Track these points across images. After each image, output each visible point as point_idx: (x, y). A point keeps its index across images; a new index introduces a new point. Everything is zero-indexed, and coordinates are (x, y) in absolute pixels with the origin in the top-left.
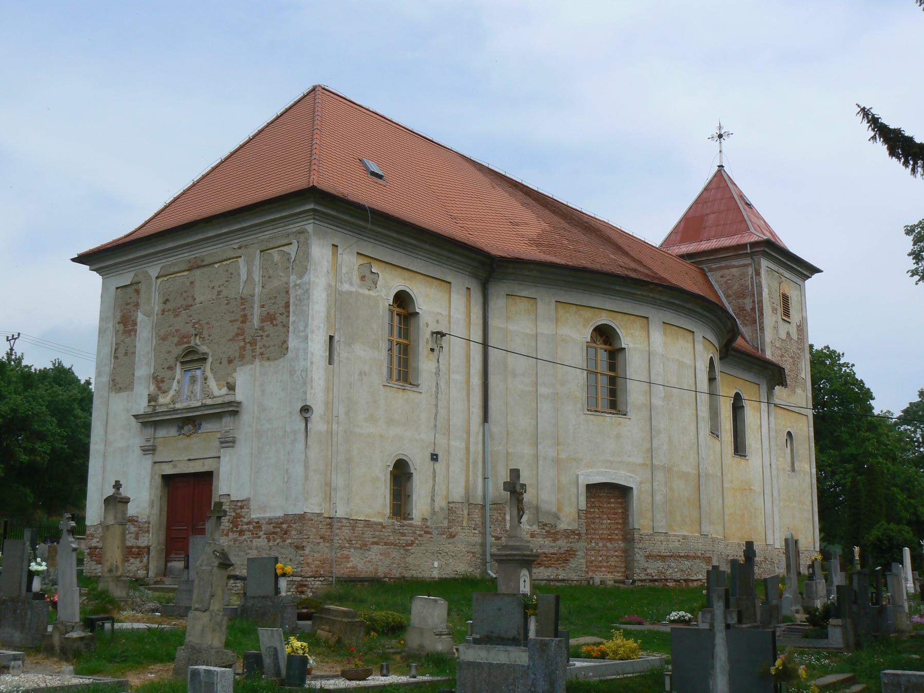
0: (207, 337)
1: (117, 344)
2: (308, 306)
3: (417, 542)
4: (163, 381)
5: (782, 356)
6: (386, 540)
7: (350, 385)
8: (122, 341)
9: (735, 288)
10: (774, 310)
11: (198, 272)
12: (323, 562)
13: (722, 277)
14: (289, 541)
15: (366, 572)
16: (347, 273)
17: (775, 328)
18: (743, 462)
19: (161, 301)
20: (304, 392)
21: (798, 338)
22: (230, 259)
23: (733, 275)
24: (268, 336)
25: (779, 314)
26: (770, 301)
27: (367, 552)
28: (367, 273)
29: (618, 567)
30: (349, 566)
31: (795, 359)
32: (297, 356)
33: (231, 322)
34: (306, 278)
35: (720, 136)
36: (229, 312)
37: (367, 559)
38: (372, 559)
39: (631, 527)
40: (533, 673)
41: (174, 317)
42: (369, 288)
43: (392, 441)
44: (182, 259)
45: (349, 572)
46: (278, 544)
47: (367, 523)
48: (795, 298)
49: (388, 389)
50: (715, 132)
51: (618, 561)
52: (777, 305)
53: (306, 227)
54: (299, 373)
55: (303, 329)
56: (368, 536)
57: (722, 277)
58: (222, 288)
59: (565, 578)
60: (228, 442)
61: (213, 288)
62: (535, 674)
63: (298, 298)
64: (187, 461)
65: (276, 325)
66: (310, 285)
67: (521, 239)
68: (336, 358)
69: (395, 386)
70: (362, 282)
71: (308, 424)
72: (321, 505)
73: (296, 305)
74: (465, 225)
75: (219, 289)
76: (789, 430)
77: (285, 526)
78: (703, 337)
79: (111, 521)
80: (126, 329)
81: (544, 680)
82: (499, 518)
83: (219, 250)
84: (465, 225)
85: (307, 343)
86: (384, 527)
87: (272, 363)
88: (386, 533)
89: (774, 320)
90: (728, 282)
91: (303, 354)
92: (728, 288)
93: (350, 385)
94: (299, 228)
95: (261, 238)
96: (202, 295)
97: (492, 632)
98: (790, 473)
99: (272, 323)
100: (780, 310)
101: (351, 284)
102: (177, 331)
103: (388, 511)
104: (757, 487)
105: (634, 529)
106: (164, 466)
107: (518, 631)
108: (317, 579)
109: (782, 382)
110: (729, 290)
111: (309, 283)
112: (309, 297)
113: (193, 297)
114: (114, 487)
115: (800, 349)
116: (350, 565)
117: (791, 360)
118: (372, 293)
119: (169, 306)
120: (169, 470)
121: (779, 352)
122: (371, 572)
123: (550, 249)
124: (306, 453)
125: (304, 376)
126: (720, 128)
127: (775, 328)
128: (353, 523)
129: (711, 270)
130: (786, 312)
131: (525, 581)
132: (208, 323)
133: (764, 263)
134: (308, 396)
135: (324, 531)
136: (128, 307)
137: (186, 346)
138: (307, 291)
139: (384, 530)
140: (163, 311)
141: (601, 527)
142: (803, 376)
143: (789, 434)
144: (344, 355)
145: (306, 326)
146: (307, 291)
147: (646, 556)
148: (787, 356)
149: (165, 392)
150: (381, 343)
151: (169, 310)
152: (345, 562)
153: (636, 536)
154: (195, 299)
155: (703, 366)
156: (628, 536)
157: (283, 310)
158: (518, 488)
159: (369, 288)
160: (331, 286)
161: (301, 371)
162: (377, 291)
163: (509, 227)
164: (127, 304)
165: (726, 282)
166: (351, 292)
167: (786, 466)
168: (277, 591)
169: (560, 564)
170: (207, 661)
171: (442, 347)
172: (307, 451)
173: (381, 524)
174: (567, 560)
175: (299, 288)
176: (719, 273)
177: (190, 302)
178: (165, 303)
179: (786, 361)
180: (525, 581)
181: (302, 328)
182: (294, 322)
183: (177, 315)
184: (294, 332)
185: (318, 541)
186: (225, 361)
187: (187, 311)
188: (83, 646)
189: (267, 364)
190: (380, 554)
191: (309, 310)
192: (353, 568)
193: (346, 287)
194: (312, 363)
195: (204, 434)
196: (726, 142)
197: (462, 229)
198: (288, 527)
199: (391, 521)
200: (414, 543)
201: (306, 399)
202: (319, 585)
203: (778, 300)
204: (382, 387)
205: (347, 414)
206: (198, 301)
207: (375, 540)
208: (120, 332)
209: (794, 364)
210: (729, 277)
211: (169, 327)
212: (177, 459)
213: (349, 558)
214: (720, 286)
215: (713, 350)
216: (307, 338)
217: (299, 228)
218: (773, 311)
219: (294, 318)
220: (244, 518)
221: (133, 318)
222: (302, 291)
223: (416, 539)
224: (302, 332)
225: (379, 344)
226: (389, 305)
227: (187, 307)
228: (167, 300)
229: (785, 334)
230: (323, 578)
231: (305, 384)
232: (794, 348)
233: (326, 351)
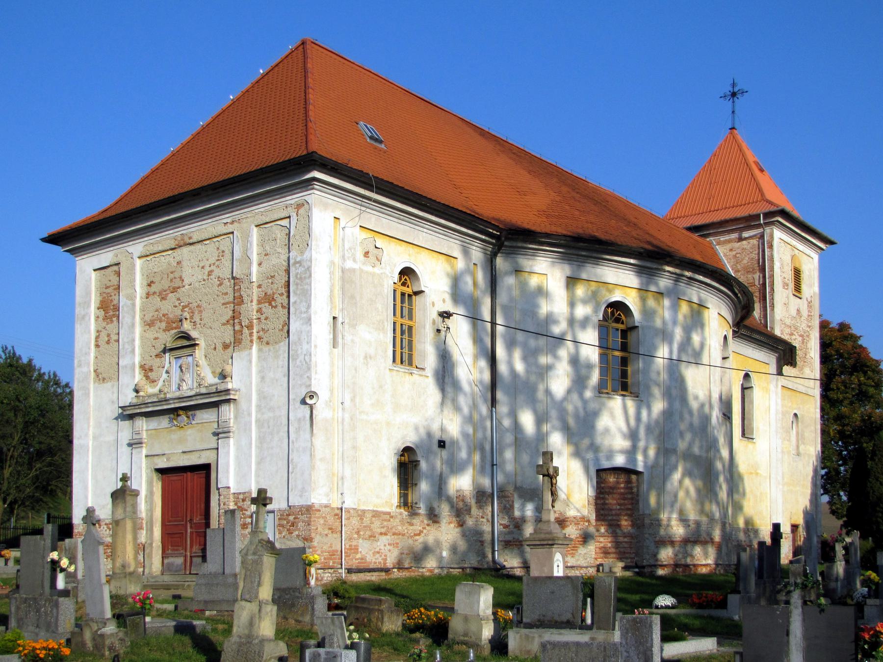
0: (198, 321)
1: (98, 331)
2: (310, 285)
3: (425, 531)
4: (151, 370)
5: (792, 334)
6: (394, 530)
7: (356, 370)
8: (105, 328)
9: (745, 262)
10: (786, 285)
11: (185, 250)
12: (332, 554)
13: (731, 250)
14: (297, 533)
15: (375, 563)
16: (350, 249)
17: (785, 304)
18: (750, 445)
19: (145, 283)
20: (308, 377)
21: (809, 316)
22: (220, 235)
23: (743, 249)
24: (266, 319)
25: (790, 290)
26: (781, 276)
27: (375, 542)
28: (371, 249)
29: (627, 553)
30: (357, 557)
31: (805, 337)
32: (299, 339)
33: (223, 304)
34: (306, 255)
35: (734, 95)
36: (223, 294)
37: (376, 550)
38: (380, 549)
39: (641, 512)
40: (626, 651)
41: (161, 301)
42: (373, 265)
43: (398, 428)
44: (168, 236)
45: (359, 563)
46: (284, 537)
47: (376, 514)
48: (807, 272)
49: (395, 373)
50: (728, 89)
51: (627, 547)
52: (788, 280)
53: (306, 198)
54: (301, 358)
55: (305, 310)
56: (377, 526)
57: (731, 250)
58: (213, 268)
59: (575, 565)
60: (221, 433)
61: (203, 267)
62: (628, 652)
63: (299, 276)
64: (182, 454)
65: (276, 307)
66: (311, 262)
67: (530, 210)
68: (340, 340)
69: (401, 370)
70: (366, 259)
71: (314, 411)
72: (328, 496)
73: (297, 284)
74: (470, 195)
75: (211, 269)
76: (795, 411)
77: (291, 518)
78: (718, 313)
79: (120, 514)
80: (107, 315)
81: (638, 658)
82: (507, 505)
83: (207, 226)
84: (470, 195)
85: (311, 325)
86: (392, 517)
87: (272, 348)
88: (395, 522)
89: (785, 295)
90: (738, 255)
91: (306, 337)
92: (737, 263)
93: (356, 370)
94: (297, 200)
95: (256, 211)
96: (191, 275)
97: (544, 616)
98: (795, 456)
99: (270, 304)
100: (792, 285)
101: (354, 261)
102: (164, 315)
103: (395, 500)
104: (763, 471)
105: (645, 514)
106: (156, 459)
107: (572, 614)
108: (326, 571)
109: (792, 363)
110: (738, 265)
111: (311, 261)
112: (310, 276)
113: (181, 277)
114: (121, 480)
115: (809, 327)
116: (359, 556)
117: (800, 339)
118: (376, 270)
119: (154, 288)
120: (163, 464)
121: (787, 331)
122: (380, 563)
123: (561, 220)
124: (312, 442)
125: (308, 360)
126: (734, 85)
127: (785, 304)
128: (362, 514)
129: (719, 243)
130: (798, 288)
131: (558, 566)
132: (198, 306)
133: (778, 234)
134: (313, 382)
135: (331, 520)
136: (108, 291)
137: (176, 331)
138: (308, 268)
139: (391, 520)
140: (148, 295)
141: (610, 513)
142: (812, 355)
143: (796, 415)
144: (348, 337)
145: (309, 307)
146: (309, 268)
147: (656, 542)
148: (796, 334)
149: (153, 381)
150: (386, 324)
151: (154, 293)
152: (354, 553)
153: (647, 521)
154: (183, 280)
155: (717, 345)
156: (639, 522)
157: (283, 290)
158: (551, 471)
159: (373, 265)
160: (334, 263)
161: (305, 355)
162: (382, 268)
163: (516, 196)
164: (107, 288)
165: (735, 256)
166: (354, 270)
167: (791, 449)
168: (307, 583)
169: (569, 551)
170: (259, 652)
171: (449, 328)
172: (313, 440)
173: (389, 513)
174: (577, 547)
175: (300, 266)
176: (729, 246)
177: (178, 283)
178: (149, 285)
179: (795, 340)
180: (558, 566)
181: (304, 309)
182: (295, 302)
183: (163, 299)
184: (295, 313)
185: (326, 532)
186: (220, 347)
187: (175, 293)
188: (117, 642)
189: (266, 348)
190: (389, 545)
191: (311, 289)
192: (362, 559)
193: (349, 264)
194: (316, 346)
195: (200, 425)
196: (740, 101)
197: (467, 199)
198: (295, 518)
199: (398, 510)
200: (422, 532)
201: (310, 385)
202: (328, 576)
203: (790, 275)
204: (388, 370)
205: (353, 400)
206: (186, 282)
207: (383, 530)
208: (101, 319)
209: (803, 343)
210: (739, 251)
211: (156, 311)
212: (170, 452)
213: (357, 549)
214: (729, 259)
215: (727, 327)
216: (310, 319)
217: (297, 200)
218: (784, 286)
219: (295, 299)
220: (246, 510)
221: (115, 302)
222: (303, 269)
223: (424, 528)
224: (304, 312)
225: (384, 326)
226: (394, 283)
227: (175, 290)
228: (152, 282)
229: (796, 311)
230: (333, 570)
231: (309, 369)
232: (804, 326)
233: (330, 333)
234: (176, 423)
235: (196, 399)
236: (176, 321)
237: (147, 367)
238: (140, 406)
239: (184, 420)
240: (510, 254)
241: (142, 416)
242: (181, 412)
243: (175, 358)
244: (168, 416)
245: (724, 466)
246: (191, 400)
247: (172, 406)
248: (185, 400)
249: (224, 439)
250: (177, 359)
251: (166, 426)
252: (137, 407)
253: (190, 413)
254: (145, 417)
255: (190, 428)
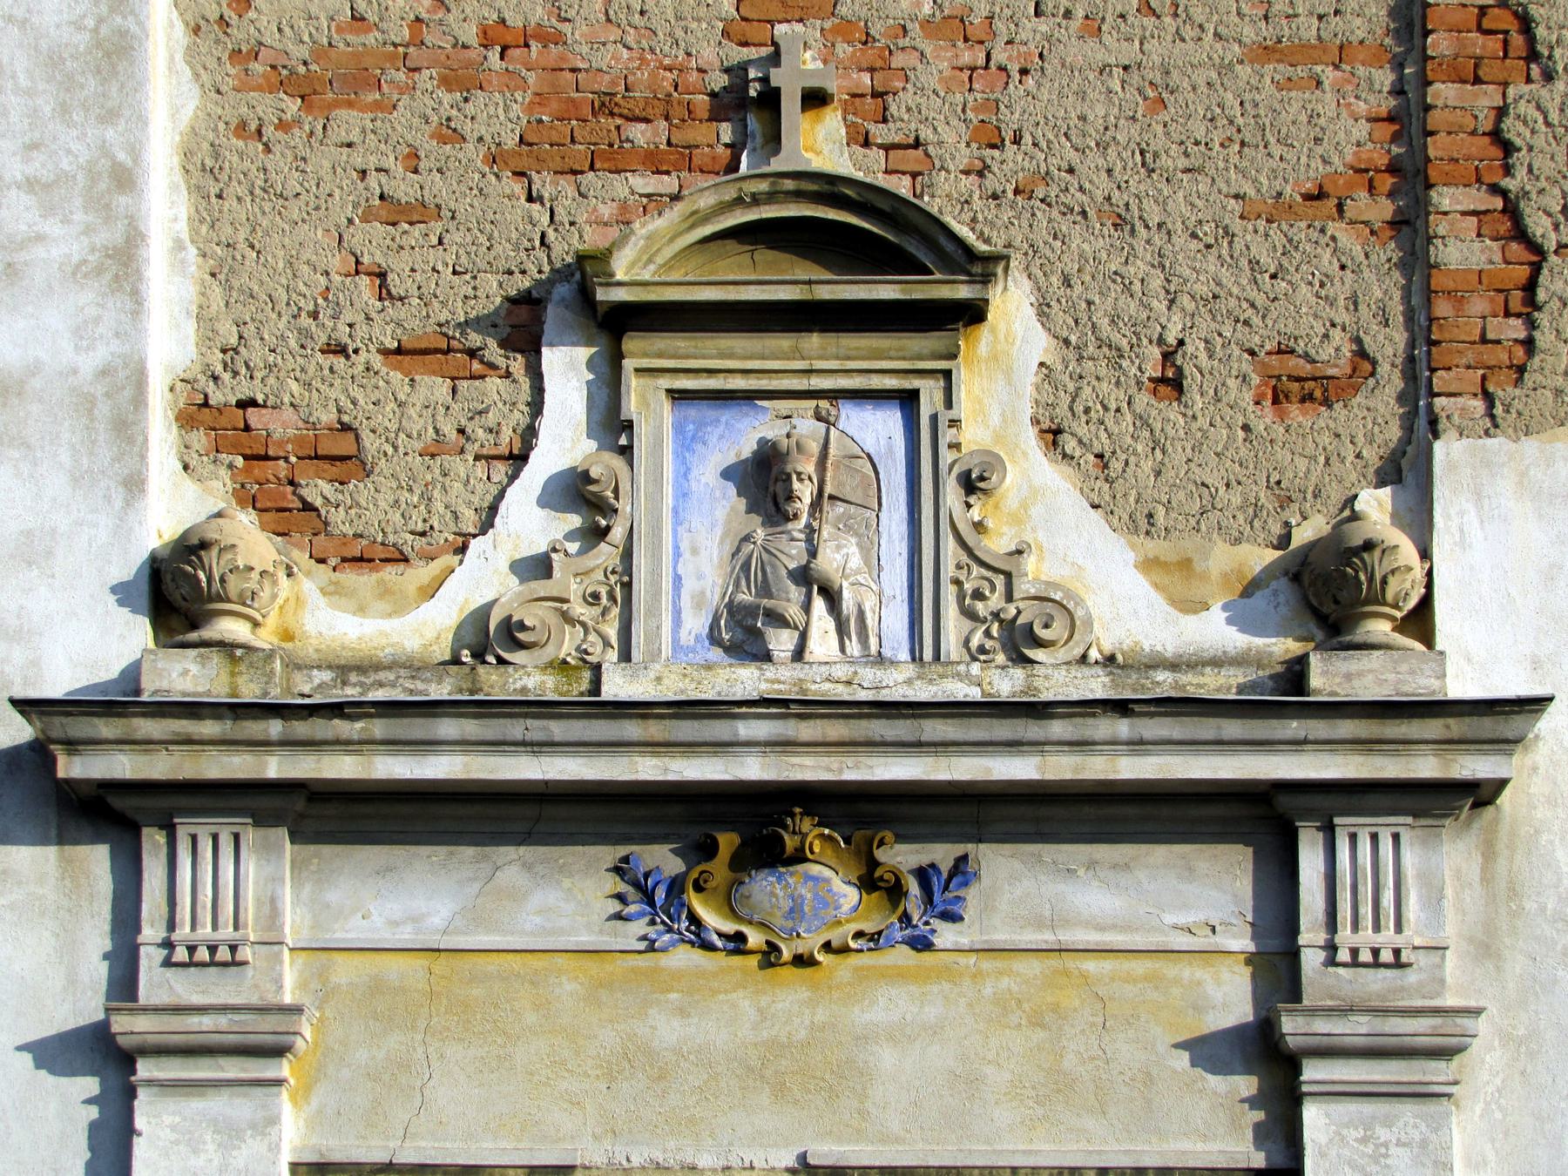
234: (714, 920)
235: (1081, 745)
236: (666, 108)
237: (278, 425)
238: (302, 728)
239: (826, 900)
240: (389, 869)
241: (262, 820)
242: (808, 831)
243: (677, 396)
244: (610, 854)
245: (653, 203)
246: (1013, 746)
247: (752, 769)
248: (936, 729)
249: (1367, 1108)
250: (693, 411)
251: (585, 939)
252: (275, 728)
253: (901, 857)
254: (295, 837)
255: (899, 975)
